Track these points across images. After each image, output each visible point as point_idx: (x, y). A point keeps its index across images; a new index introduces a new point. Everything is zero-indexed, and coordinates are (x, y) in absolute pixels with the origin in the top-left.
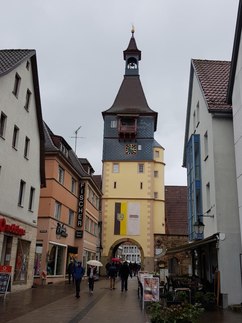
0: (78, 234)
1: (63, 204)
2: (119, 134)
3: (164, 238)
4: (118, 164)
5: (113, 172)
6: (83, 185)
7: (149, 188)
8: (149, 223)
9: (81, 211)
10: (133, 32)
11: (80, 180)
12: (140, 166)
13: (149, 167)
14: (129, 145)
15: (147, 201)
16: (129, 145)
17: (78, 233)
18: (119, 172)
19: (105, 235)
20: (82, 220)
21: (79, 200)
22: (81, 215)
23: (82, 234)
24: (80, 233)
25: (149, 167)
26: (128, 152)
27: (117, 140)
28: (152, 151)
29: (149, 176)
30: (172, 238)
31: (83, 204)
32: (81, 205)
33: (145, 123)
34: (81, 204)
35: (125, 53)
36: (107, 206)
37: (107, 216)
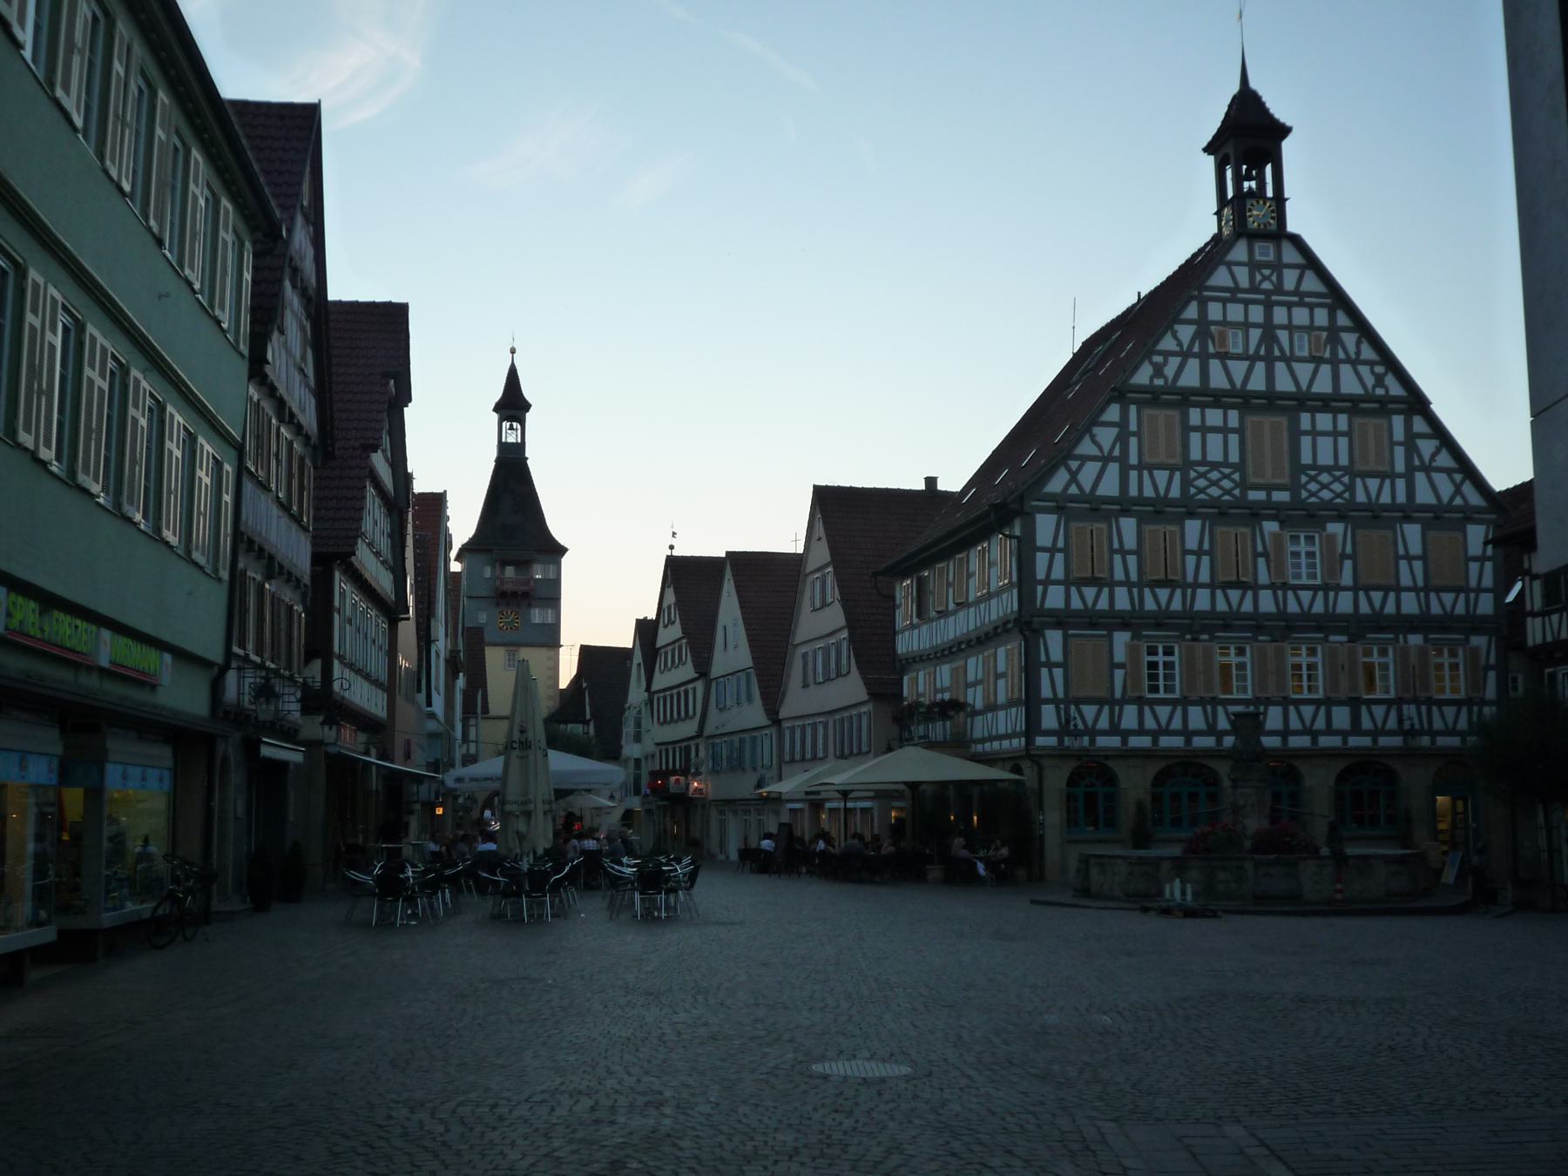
10: (513, 351)
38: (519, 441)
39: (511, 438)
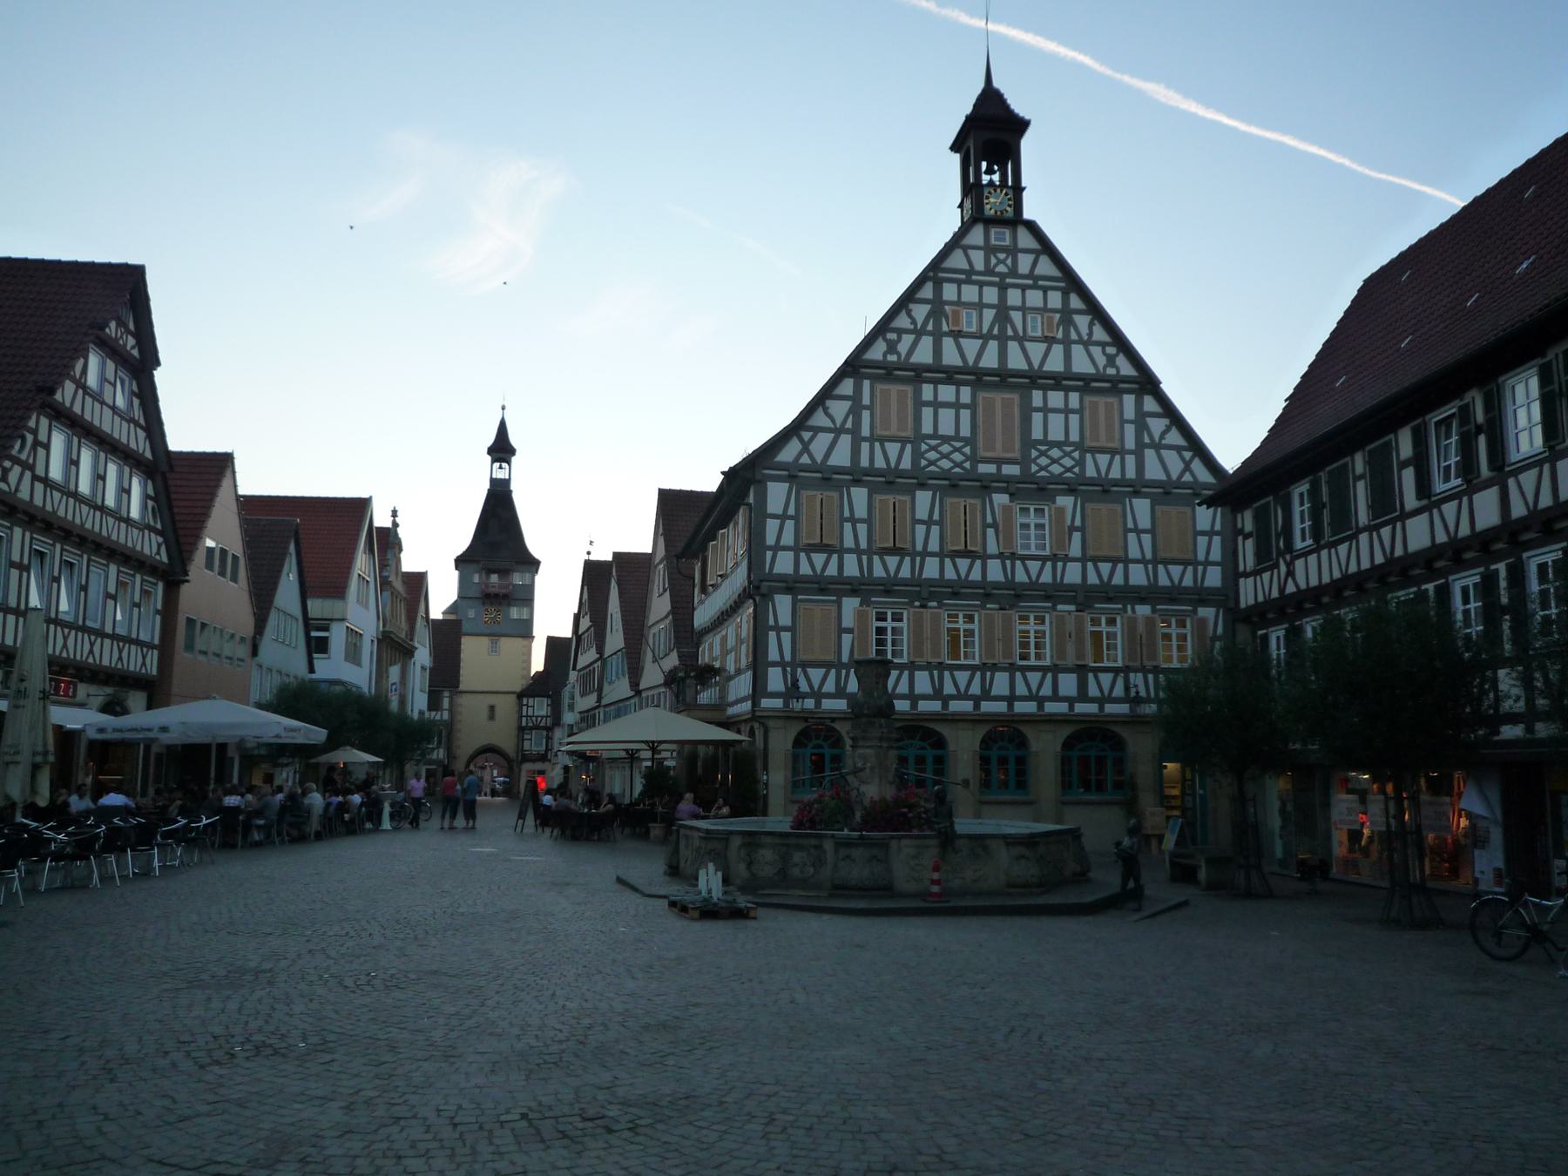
10: (503, 408)
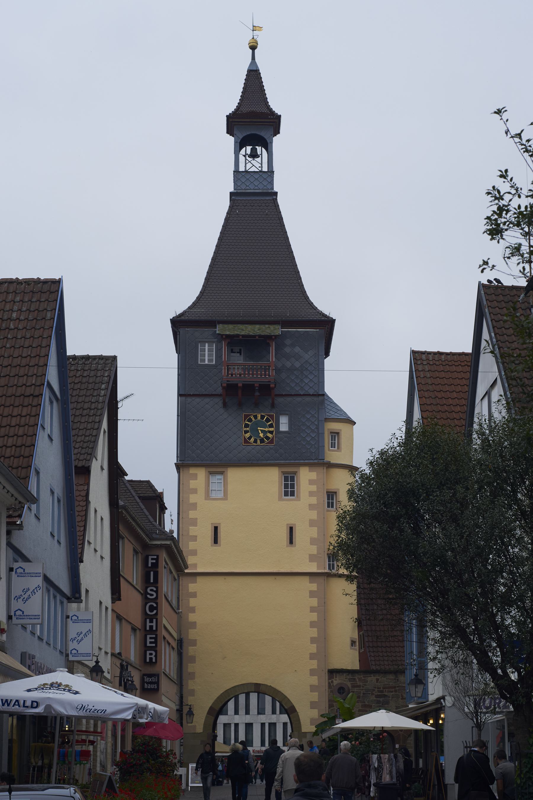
0: (148, 683)
1: (125, 617)
2: (223, 388)
3: (357, 680)
4: (222, 473)
5: (208, 497)
6: (154, 561)
7: (313, 541)
8: (313, 640)
9: (151, 627)
10: (253, 48)
11: (145, 546)
12: (286, 479)
13: (311, 482)
14: (252, 417)
15: (307, 579)
16: (252, 417)
17: (147, 679)
18: (225, 498)
19: (192, 676)
20: (154, 649)
21: (146, 598)
22: (154, 636)
23: (158, 683)
24: (154, 679)
25: (311, 482)
26: (250, 438)
27: (219, 401)
28: (320, 435)
29: (311, 507)
30: (377, 680)
31: (156, 608)
32: (151, 611)
33: (297, 349)
34: (152, 608)
35: (231, 120)
36: (194, 595)
37: (196, 622)
38: (265, 169)
39: (254, 165)
